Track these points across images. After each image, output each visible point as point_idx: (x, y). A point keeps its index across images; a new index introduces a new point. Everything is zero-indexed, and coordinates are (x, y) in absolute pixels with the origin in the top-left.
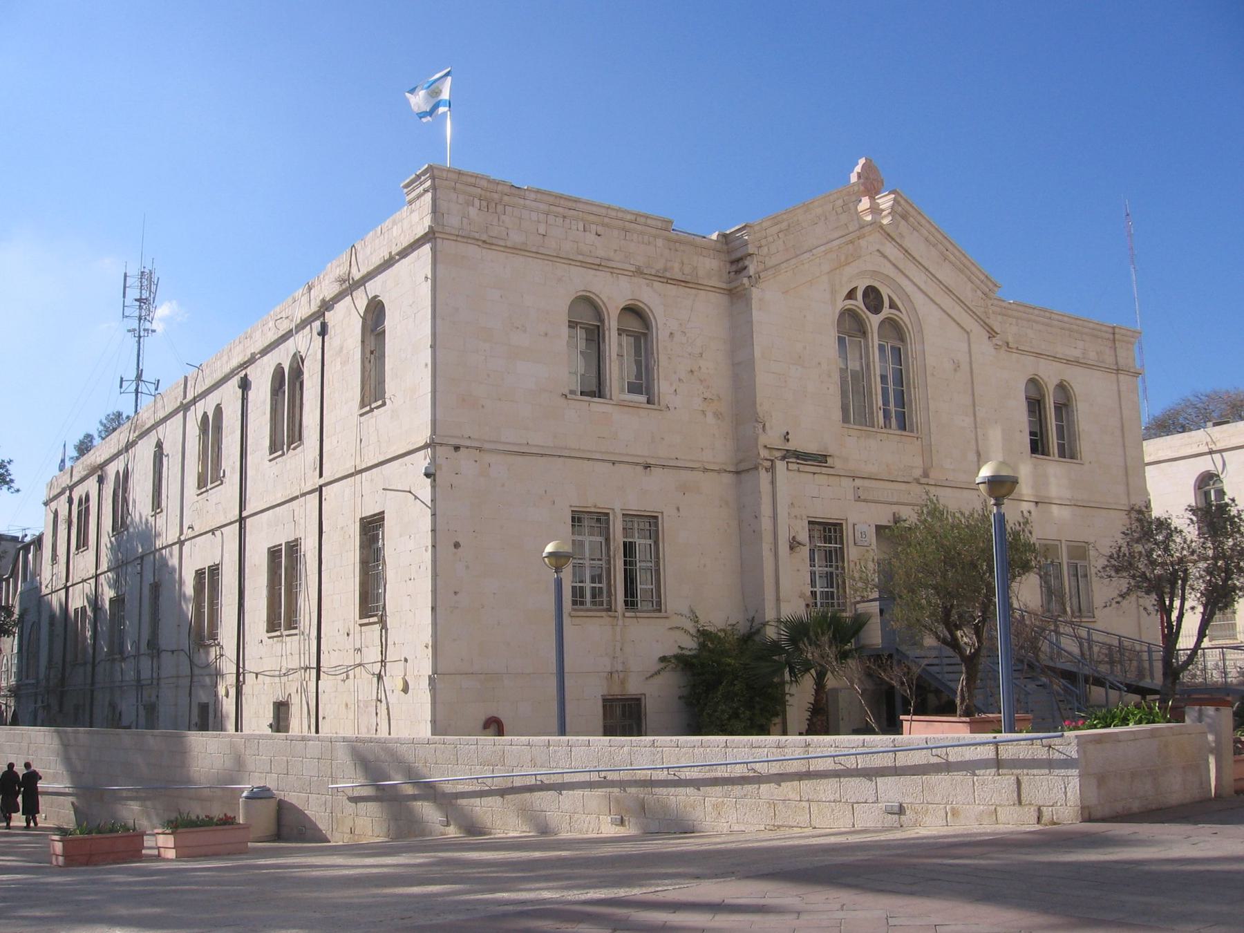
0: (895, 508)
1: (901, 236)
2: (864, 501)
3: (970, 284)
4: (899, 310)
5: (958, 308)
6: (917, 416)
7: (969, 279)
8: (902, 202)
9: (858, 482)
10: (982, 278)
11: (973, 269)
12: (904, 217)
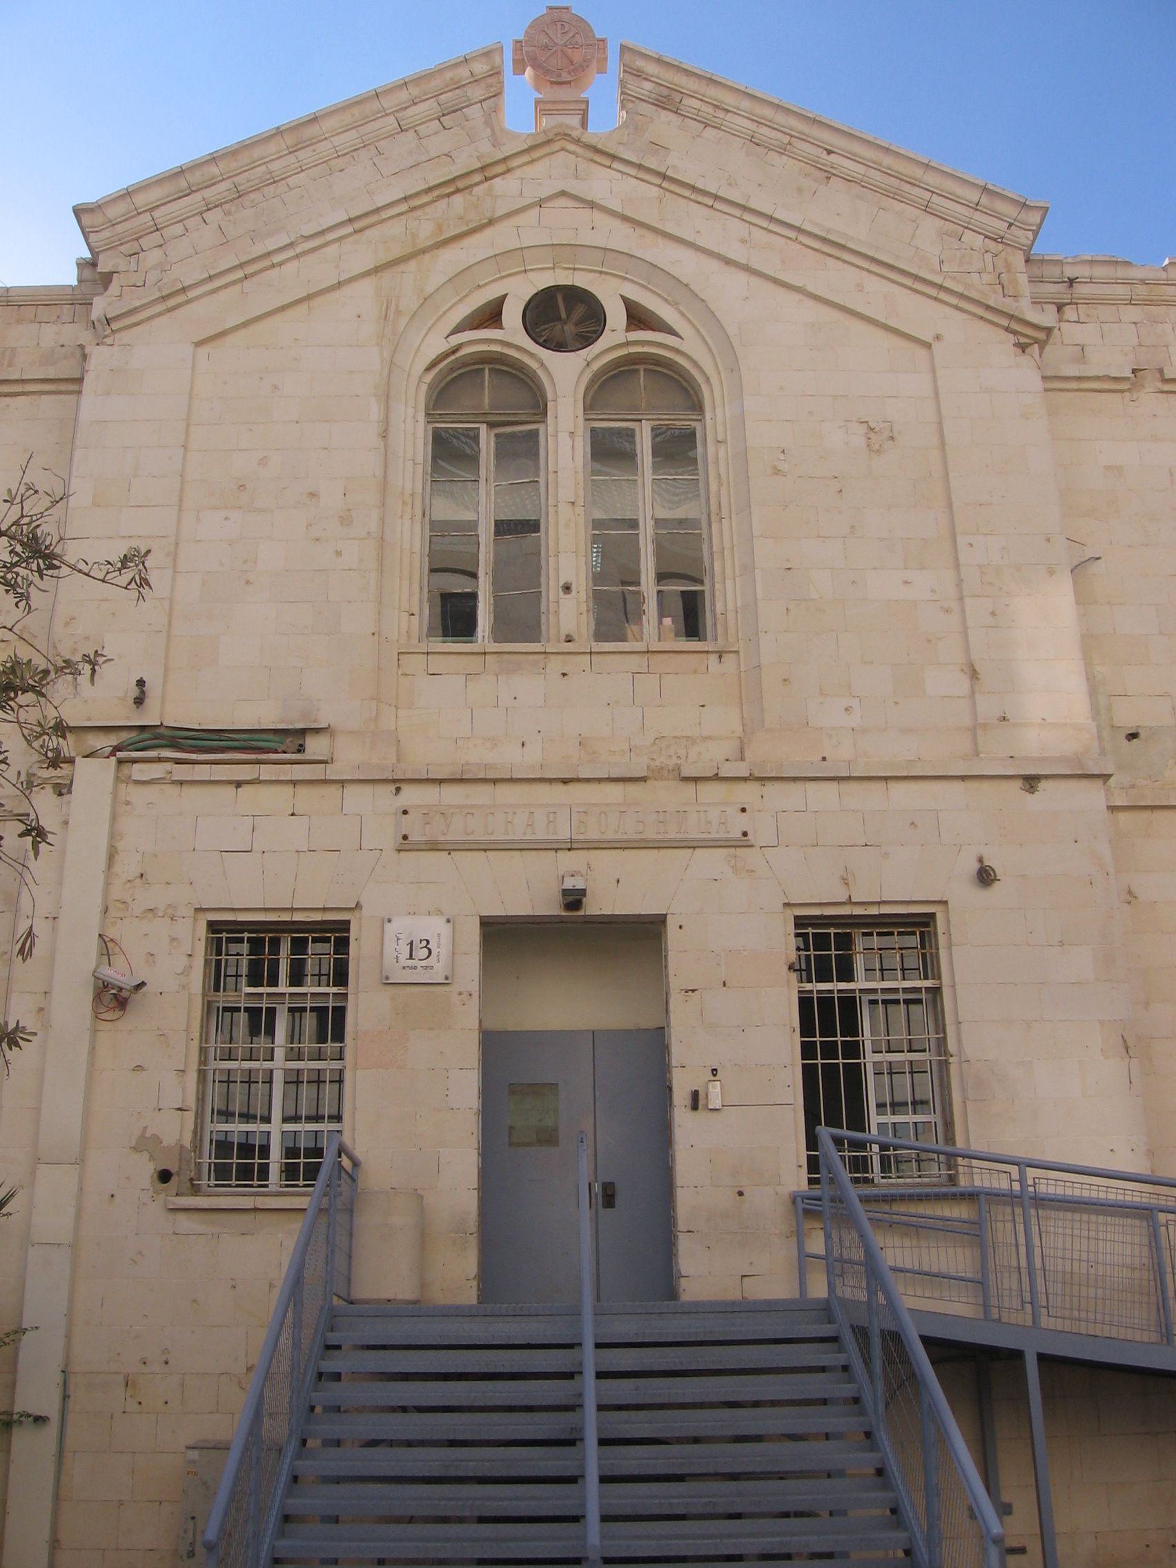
0: (568, 861)
1: (656, 146)
2: (433, 846)
3: (931, 225)
4: (671, 331)
5: (874, 285)
6: (725, 598)
7: (927, 209)
8: (651, 68)
9: (411, 795)
10: (974, 196)
11: (932, 179)
12: (667, 102)
